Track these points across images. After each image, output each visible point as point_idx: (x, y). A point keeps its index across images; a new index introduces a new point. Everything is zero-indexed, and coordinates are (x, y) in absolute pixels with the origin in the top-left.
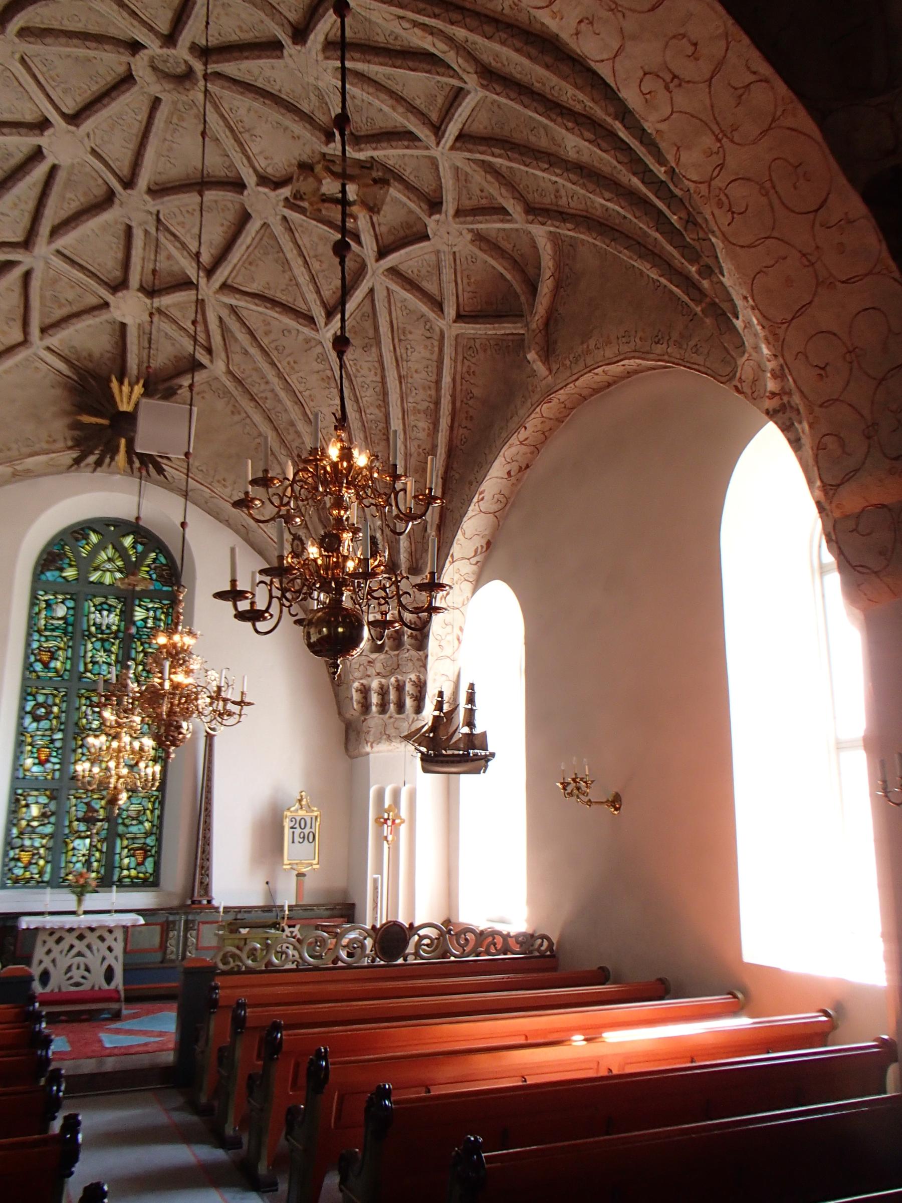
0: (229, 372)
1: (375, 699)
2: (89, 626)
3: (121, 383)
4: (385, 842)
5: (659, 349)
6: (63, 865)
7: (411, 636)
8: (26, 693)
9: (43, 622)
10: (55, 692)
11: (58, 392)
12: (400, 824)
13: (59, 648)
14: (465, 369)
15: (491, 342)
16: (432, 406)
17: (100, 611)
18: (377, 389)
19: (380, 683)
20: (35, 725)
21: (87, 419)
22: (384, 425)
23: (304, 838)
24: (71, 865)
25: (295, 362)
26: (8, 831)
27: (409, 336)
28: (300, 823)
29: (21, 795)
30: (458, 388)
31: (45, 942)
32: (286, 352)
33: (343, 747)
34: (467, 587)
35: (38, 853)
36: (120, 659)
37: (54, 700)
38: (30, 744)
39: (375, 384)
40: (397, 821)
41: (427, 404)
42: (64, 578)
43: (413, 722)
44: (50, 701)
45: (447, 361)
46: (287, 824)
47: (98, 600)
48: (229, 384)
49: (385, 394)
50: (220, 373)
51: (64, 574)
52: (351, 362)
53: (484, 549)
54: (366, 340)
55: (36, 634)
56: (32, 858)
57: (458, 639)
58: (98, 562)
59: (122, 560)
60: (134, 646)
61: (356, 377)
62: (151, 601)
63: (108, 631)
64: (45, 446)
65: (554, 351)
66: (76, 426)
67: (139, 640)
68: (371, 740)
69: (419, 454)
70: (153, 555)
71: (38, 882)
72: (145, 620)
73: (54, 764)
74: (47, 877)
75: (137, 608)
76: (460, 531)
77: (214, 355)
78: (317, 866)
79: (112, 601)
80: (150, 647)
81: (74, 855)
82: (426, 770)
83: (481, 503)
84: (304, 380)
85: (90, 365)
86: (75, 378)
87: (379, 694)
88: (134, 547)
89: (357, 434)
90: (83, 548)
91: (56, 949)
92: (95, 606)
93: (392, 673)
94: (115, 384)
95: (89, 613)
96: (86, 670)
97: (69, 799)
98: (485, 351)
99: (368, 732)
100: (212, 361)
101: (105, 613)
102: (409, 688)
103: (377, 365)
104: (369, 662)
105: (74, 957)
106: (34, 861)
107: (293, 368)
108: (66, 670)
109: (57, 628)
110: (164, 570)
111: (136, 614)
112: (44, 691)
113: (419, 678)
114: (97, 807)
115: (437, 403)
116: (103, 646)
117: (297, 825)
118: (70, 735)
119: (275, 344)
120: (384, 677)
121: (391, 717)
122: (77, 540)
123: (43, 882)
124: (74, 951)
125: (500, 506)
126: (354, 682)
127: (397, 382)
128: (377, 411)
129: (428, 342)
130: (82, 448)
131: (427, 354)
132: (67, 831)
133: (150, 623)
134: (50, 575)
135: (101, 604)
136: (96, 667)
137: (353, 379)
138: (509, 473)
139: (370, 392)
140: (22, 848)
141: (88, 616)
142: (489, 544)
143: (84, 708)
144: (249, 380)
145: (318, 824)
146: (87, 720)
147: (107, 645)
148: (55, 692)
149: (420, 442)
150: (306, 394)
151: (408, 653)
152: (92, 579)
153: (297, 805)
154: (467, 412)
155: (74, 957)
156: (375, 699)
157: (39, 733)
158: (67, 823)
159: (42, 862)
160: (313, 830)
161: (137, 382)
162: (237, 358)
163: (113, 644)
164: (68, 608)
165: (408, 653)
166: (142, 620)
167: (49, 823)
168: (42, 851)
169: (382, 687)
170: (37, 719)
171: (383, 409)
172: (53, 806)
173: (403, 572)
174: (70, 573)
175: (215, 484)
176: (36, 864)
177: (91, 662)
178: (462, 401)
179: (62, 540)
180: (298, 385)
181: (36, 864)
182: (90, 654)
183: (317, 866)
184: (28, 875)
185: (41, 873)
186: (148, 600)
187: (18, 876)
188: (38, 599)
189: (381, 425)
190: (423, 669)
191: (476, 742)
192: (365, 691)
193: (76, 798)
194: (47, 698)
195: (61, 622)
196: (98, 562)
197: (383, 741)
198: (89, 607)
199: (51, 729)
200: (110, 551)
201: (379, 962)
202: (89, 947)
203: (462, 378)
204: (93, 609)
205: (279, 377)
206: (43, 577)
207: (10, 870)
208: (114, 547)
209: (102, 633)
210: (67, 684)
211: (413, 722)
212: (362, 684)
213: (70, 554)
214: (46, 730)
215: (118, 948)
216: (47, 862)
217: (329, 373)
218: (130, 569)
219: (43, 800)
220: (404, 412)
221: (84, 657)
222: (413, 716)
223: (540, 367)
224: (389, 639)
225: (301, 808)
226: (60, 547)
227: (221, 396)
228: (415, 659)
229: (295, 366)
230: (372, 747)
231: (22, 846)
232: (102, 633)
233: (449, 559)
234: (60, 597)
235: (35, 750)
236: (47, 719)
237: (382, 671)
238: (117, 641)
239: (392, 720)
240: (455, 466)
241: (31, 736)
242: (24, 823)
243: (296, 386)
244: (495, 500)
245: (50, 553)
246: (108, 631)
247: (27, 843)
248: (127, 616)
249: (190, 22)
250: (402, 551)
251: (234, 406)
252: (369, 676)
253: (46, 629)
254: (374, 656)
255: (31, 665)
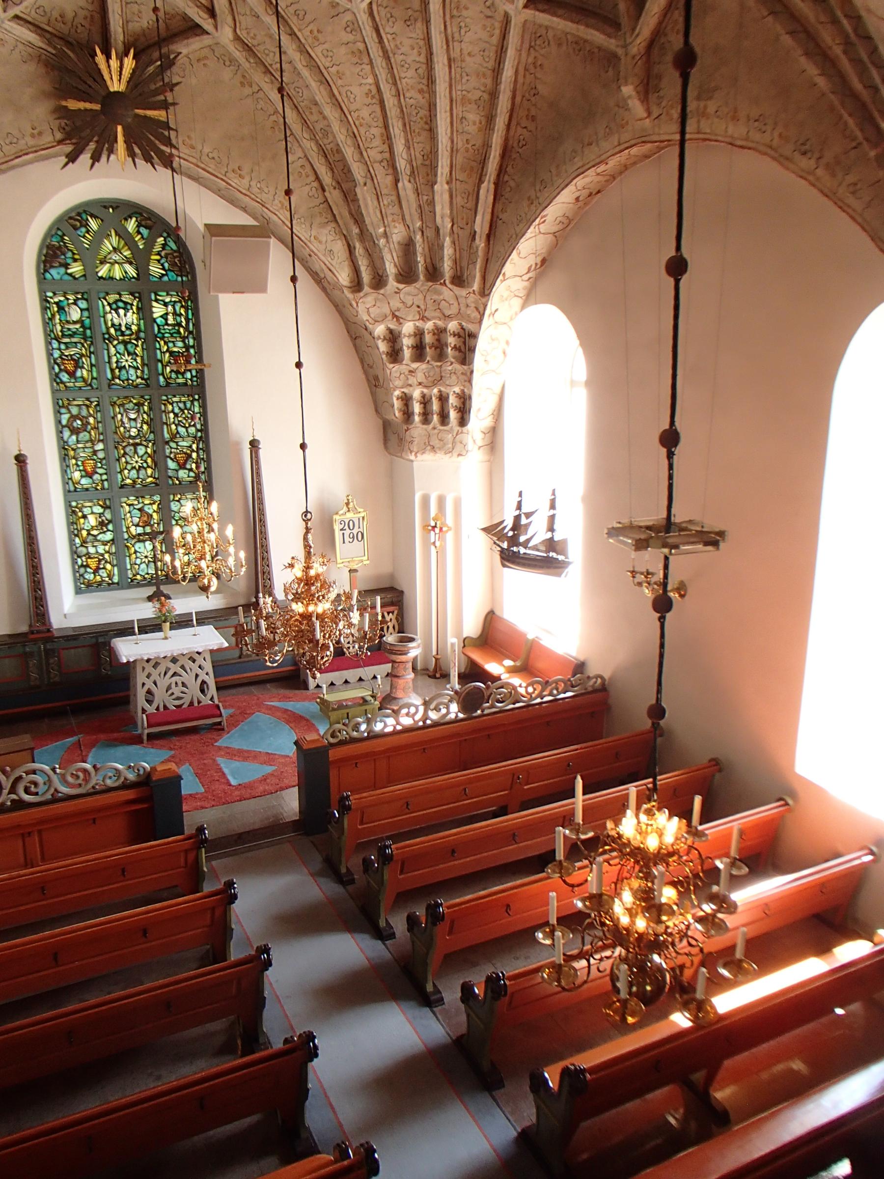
0: (237, 38)
1: (417, 408)
2: (108, 328)
3: (108, 57)
4: (433, 547)
5: (806, 163)
6: (129, 567)
7: (455, 348)
8: (59, 407)
9: (59, 328)
10: (88, 403)
11: (31, 67)
12: (447, 531)
13: (82, 355)
14: (531, 60)
15: (569, 37)
16: (486, 96)
17: (116, 310)
18: (420, 71)
19: (422, 392)
20: (74, 437)
21: (73, 105)
22: (427, 113)
23: (353, 537)
24: (137, 567)
25: (318, 31)
26: (72, 543)
27: (465, 13)
28: (350, 524)
29: (76, 507)
30: (521, 80)
31: (144, 669)
32: (308, 18)
33: (382, 446)
34: (517, 303)
35: (104, 559)
36: (146, 362)
37: (88, 411)
38: (74, 458)
39: (418, 65)
40: (445, 529)
41: (480, 94)
42: (70, 275)
43: (457, 434)
44: (84, 412)
45: (511, 53)
46: (337, 527)
47: (112, 298)
48: (239, 55)
49: (431, 80)
50: (227, 41)
51: (69, 271)
52: (389, 36)
53: (538, 266)
54: (410, 12)
55: (54, 341)
56: (99, 564)
57: (504, 353)
58: (103, 253)
59: (129, 249)
60: (158, 346)
61: (394, 54)
62: (168, 294)
63: (128, 332)
64: (31, 142)
65: (657, 89)
66: (62, 112)
67: (162, 338)
68: (415, 450)
69: (467, 151)
70: (161, 240)
71: (109, 584)
72: (165, 316)
73: (101, 475)
74: (116, 579)
75: (154, 304)
76: (515, 252)
77: (219, 19)
78: (368, 562)
79: (127, 298)
80: (175, 346)
81: (137, 558)
82: (504, 566)
83: (541, 226)
84: (330, 54)
85: (65, 29)
86: (92, 146)
87: (421, 403)
88: (139, 232)
89: (395, 124)
90: (84, 237)
91: (155, 674)
92: (109, 304)
93: (434, 384)
94: (100, 58)
95: (105, 313)
96: (113, 378)
97: (122, 506)
98: (560, 45)
99: (412, 442)
100: (216, 28)
101: (122, 312)
102: (453, 400)
103: (422, 43)
104: (410, 371)
105: (172, 676)
106: (101, 566)
107: (317, 39)
108: (93, 378)
109: (75, 333)
110: (175, 257)
111: (154, 310)
112: (75, 403)
113: (463, 391)
114: (150, 512)
115: (494, 95)
116: (126, 349)
117: (346, 527)
118: (111, 445)
119: (294, 7)
120: (426, 387)
121: (434, 428)
122: (76, 228)
123: (113, 583)
124: (170, 673)
125: (561, 227)
126: (395, 390)
127: (447, 69)
128: (419, 97)
129: (488, 22)
130: (74, 141)
131: (484, 35)
132: (126, 536)
133: (171, 320)
134: (56, 273)
135: (116, 302)
136: (124, 372)
137: (391, 55)
138: (577, 199)
139: (411, 73)
140: (88, 556)
141: (104, 317)
142: (544, 261)
143: (119, 416)
144: (261, 48)
145: (365, 523)
146: (125, 428)
147: (131, 349)
148: (88, 403)
149: (469, 137)
150: (333, 70)
151: (452, 366)
152: (100, 274)
153: (345, 509)
154: (528, 110)
155: (172, 676)
156: (417, 408)
157: (80, 446)
158: (125, 530)
159: (108, 566)
160: (361, 530)
161: (126, 54)
162: (245, 21)
163: (137, 346)
164: (82, 310)
165: (452, 366)
166: (161, 317)
167: (108, 530)
168: (107, 556)
169: (423, 396)
170: (75, 431)
171: (427, 95)
172: (108, 515)
173: (447, 282)
174: (76, 269)
175: (231, 175)
176: (104, 568)
177: (117, 367)
178: (523, 96)
179: (58, 229)
180: (323, 60)
181: (104, 568)
182: (114, 359)
183: (368, 562)
184: (98, 578)
185: (110, 576)
186: (164, 294)
187: (89, 581)
188: (48, 302)
189: (424, 113)
190: (467, 384)
191: (558, 548)
192: (406, 400)
193: (129, 505)
194: (80, 409)
195: (78, 326)
196: (103, 253)
197: (427, 452)
198: (104, 306)
199: (91, 441)
200: (114, 240)
201: (461, 716)
202: (183, 667)
203: (526, 70)
204: (108, 308)
205: (301, 52)
206: (48, 276)
207: (82, 575)
208: (117, 234)
209: (123, 334)
210: (98, 393)
211: (457, 434)
212: (403, 392)
213: (71, 246)
214: (87, 442)
215: (208, 666)
216: (113, 566)
217: (361, 46)
218: (140, 260)
219: (98, 510)
220: (451, 101)
221: (109, 362)
222: (457, 428)
223: (637, 107)
224: (430, 348)
225: (349, 511)
226: (59, 239)
227: (227, 63)
228: (459, 373)
229: (320, 36)
230: (416, 457)
231: (88, 553)
232: (123, 334)
233: (501, 277)
234: (71, 298)
235: (80, 463)
236: (85, 430)
237: (424, 381)
238: (140, 343)
239: (436, 431)
240: (509, 169)
241: (73, 449)
242: (84, 533)
243: (322, 62)
244: (557, 221)
245: (50, 247)
246: (128, 332)
247: (92, 550)
248: (144, 311)
249: (750, 1013)
250: (446, 258)
251: (244, 76)
252: (411, 386)
253: (63, 336)
254: (415, 365)
255: (57, 375)
